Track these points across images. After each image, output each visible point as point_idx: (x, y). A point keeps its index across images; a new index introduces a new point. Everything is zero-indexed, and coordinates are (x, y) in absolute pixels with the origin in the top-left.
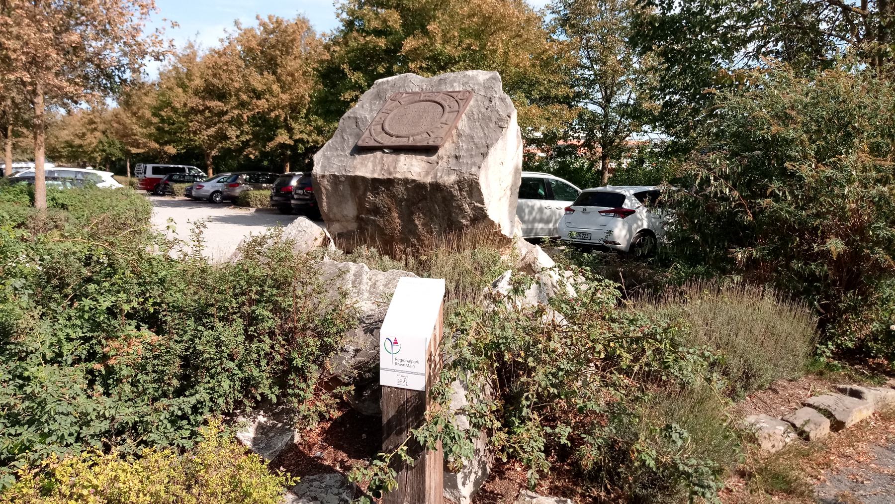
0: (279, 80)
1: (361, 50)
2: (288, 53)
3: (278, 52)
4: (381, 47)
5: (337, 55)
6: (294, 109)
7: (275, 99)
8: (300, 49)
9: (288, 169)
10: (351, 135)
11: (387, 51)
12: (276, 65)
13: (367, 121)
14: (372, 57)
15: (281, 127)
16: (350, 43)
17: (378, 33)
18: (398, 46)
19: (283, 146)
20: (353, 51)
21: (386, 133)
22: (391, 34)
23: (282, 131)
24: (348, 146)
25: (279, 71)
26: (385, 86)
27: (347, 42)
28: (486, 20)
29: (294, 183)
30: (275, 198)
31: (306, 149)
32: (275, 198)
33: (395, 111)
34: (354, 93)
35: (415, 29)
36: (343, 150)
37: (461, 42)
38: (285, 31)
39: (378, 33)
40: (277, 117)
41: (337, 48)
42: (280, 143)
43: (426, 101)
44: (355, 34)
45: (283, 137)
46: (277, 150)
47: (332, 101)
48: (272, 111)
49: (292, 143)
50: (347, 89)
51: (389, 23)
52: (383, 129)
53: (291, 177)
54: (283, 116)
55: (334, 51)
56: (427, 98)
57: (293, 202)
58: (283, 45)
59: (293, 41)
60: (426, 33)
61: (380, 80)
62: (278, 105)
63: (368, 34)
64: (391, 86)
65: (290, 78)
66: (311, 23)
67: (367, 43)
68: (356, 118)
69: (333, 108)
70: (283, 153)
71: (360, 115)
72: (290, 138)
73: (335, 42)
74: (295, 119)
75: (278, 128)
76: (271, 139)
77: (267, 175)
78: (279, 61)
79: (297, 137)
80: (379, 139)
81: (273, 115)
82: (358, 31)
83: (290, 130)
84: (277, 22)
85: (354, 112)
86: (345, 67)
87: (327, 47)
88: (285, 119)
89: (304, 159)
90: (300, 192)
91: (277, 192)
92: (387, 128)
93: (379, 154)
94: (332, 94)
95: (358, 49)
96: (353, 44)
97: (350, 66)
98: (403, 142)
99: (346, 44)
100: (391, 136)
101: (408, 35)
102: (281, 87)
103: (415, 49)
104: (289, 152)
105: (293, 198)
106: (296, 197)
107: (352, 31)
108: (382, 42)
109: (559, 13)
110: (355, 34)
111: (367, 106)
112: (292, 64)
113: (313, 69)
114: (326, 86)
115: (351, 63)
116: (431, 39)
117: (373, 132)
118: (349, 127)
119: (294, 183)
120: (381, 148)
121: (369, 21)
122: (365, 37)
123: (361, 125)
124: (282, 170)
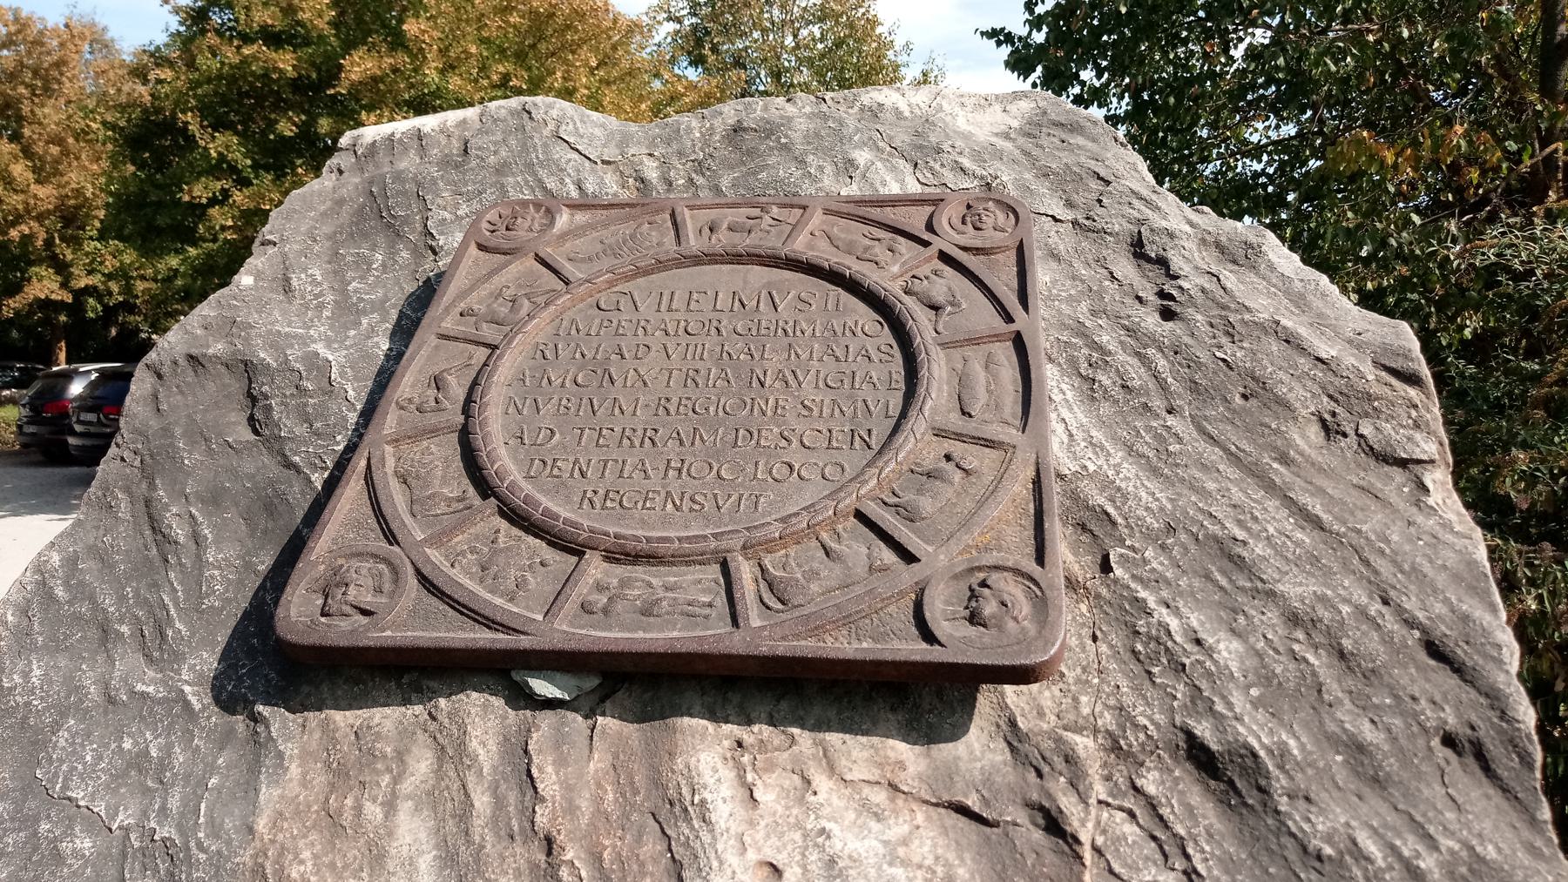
0: (27, 152)
1: (232, 80)
2: (48, 91)
3: (22, 90)
4: (281, 71)
5: (166, 89)
6: (70, 218)
7: (21, 197)
8: (81, 81)
9: (62, 356)
10: (214, 499)
11: (297, 85)
12: (20, 119)
13: (329, 389)
14: (260, 98)
15: (39, 262)
16: (200, 60)
17: (273, 39)
18: (332, 72)
19: (46, 305)
20: (209, 81)
21: (516, 517)
22: (307, 42)
23: (42, 270)
24: (195, 609)
25: (26, 132)
26: (408, 163)
27: (193, 58)
28: (539, 23)
29: (76, 388)
30: (31, 429)
31: (106, 307)
32: (31, 429)
33: (538, 329)
34: (218, 185)
35: (369, 33)
36: (156, 645)
37: (483, 69)
38: (38, 42)
39: (273, 39)
40: (27, 239)
41: (166, 74)
42: (37, 300)
43: (736, 258)
44: (212, 39)
45: (44, 285)
46: (31, 313)
47: (159, 205)
48: (13, 224)
49: (69, 299)
50: (200, 175)
51: (300, 15)
52: (484, 487)
53: (68, 376)
54: (42, 235)
55: (159, 81)
56: (723, 240)
57: (71, 440)
58: (36, 73)
59: (60, 64)
60: (398, 41)
61: (371, 132)
62: (28, 211)
63: (246, 39)
64: (446, 162)
65: (55, 150)
66: (112, 34)
67: (245, 61)
68: (248, 369)
69: (162, 221)
70: (47, 322)
71: (277, 342)
72: (64, 286)
73: (157, 57)
74: (75, 242)
75: (31, 263)
76: (15, 289)
77: (12, 369)
78: (26, 109)
79: (82, 283)
80: (464, 580)
81: (14, 234)
82: (219, 33)
83: (61, 268)
84: (16, 20)
85: (229, 326)
86: (192, 121)
87: (139, 73)
88: (49, 243)
89: (107, 328)
90: (91, 417)
91: (36, 406)
92: (504, 461)
93: (481, 717)
94: (158, 187)
95: (220, 77)
96: (205, 62)
97: (203, 118)
98: (675, 614)
99: (191, 65)
100: (570, 545)
101: (349, 46)
102: (35, 170)
103: (375, 80)
104: (63, 318)
105: (74, 433)
106: (78, 428)
107: (203, 32)
108: (286, 62)
109: (679, 20)
110: (212, 39)
111: (312, 276)
112: (51, 114)
113: (104, 123)
114: (141, 166)
115: (204, 110)
116: (414, 57)
117: (396, 498)
118: (198, 435)
119: (76, 388)
120: (501, 671)
121: (247, 8)
122: (239, 48)
123: (289, 425)
124: (50, 360)
